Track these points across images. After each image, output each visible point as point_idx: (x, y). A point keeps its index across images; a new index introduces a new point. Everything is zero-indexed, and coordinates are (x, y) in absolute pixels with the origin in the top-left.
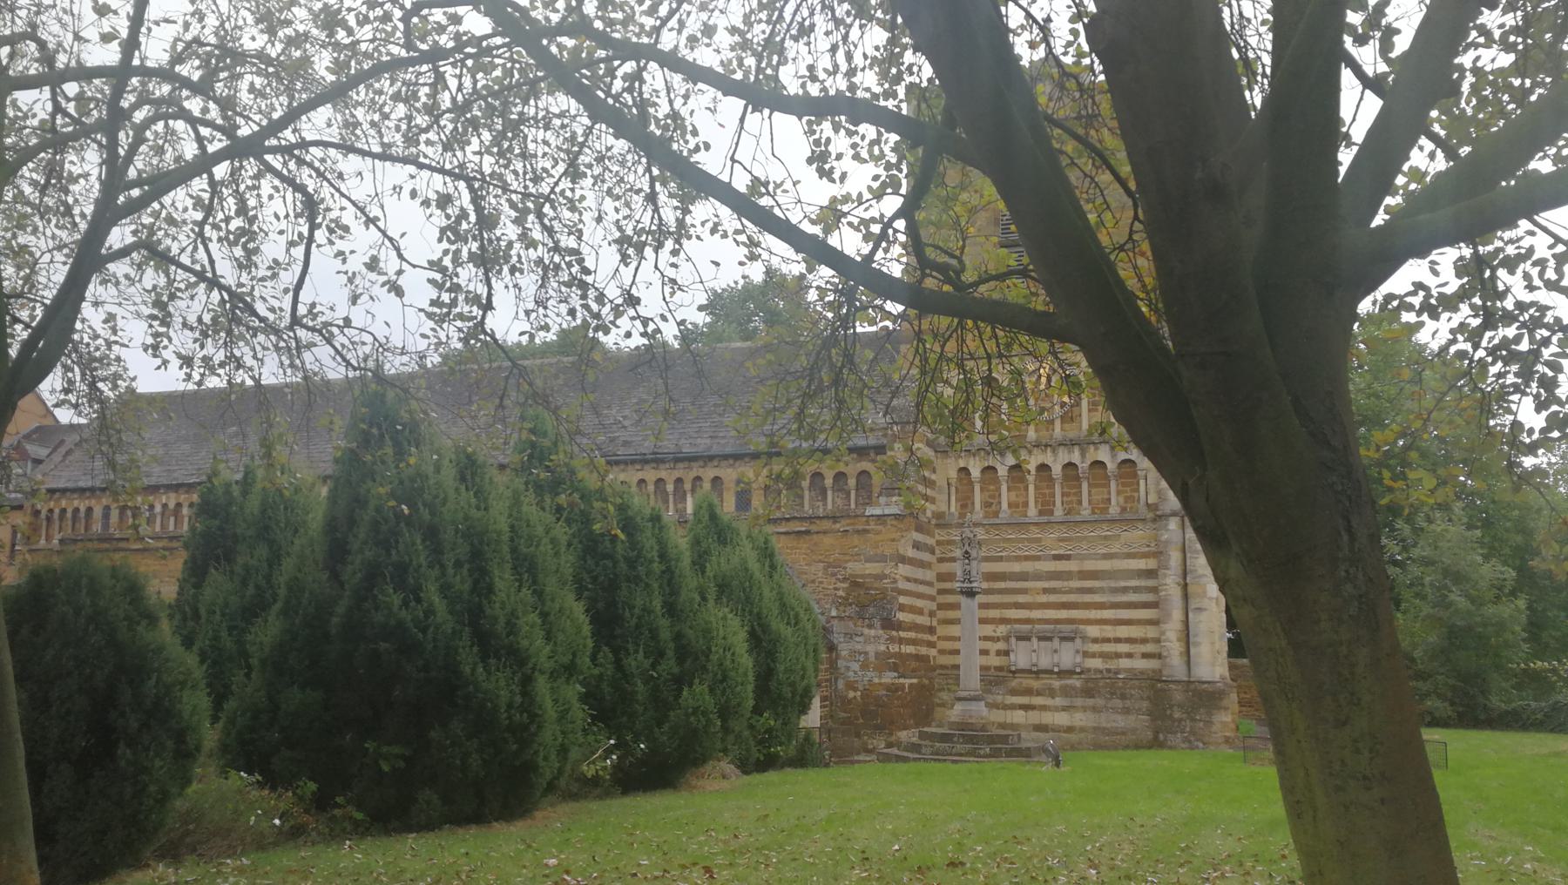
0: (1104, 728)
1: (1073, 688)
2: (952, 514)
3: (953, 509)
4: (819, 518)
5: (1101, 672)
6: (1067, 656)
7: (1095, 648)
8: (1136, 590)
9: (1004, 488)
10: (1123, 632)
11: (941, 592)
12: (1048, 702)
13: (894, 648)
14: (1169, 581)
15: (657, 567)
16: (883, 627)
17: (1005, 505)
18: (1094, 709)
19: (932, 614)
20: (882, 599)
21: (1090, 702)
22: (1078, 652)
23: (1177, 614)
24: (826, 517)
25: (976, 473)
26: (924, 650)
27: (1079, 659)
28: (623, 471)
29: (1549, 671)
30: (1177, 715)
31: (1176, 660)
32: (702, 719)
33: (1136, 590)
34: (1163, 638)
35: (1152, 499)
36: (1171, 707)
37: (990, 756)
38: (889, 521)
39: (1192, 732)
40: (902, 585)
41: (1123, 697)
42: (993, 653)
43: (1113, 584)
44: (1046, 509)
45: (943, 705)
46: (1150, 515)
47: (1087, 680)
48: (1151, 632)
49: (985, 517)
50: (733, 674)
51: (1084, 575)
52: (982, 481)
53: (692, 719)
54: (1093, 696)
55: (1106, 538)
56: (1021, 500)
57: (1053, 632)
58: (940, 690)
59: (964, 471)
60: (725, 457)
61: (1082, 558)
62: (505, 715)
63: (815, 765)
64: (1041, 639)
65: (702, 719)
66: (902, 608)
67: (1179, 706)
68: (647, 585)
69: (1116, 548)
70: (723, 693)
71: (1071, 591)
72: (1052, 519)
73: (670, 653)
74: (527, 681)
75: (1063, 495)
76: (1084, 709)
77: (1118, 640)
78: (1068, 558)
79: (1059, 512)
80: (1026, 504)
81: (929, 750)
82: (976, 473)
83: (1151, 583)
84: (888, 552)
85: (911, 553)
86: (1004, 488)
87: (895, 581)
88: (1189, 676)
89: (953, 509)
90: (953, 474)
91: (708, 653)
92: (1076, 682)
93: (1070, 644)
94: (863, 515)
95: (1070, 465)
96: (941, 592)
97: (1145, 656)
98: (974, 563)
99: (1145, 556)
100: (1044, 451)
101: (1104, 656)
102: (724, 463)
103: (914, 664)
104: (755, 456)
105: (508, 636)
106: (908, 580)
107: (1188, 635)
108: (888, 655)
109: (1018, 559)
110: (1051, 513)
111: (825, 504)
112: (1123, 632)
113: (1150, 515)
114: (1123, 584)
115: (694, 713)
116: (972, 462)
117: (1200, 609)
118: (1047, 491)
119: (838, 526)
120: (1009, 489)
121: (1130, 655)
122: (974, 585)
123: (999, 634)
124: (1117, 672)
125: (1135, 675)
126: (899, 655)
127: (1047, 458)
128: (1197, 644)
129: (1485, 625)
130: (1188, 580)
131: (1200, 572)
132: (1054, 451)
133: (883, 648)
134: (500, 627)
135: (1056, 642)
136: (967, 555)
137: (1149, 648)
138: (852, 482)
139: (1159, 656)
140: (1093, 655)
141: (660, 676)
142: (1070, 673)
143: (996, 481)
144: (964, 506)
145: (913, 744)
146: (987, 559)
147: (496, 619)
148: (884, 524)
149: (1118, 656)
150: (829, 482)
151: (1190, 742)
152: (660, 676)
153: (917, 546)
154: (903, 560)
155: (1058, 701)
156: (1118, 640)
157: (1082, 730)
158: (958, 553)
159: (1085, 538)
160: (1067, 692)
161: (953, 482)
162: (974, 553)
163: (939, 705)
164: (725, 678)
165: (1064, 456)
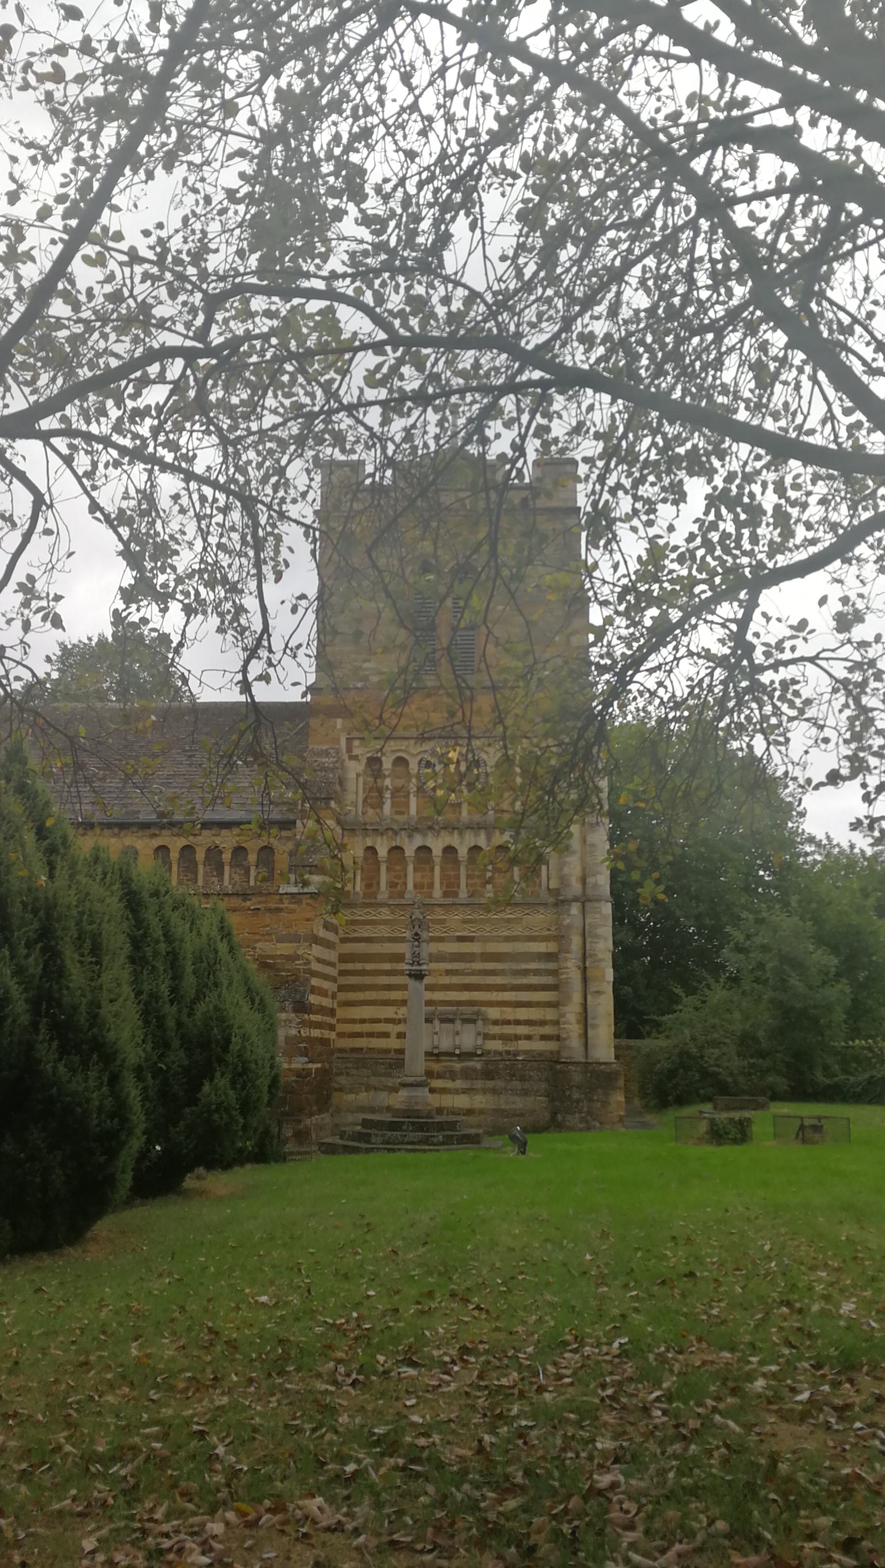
0: (503, 1110)
1: (474, 1070)
2: (356, 893)
3: (358, 889)
4: (227, 895)
5: (500, 1054)
6: (468, 1039)
7: (496, 1030)
8: (536, 972)
9: (410, 868)
10: (523, 1014)
11: (343, 973)
12: (450, 1084)
13: (305, 1032)
14: (569, 964)
15: (163, 947)
16: (295, 1011)
17: (410, 886)
18: (495, 1091)
19: (334, 996)
20: (294, 981)
21: (490, 1084)
22: (479, 1034)
23: (577, 997)
24: (236, 894)
25: (383, 852)
26: (327, 1034)
27: (480, 1041)
28: (115, 835)
29: (864, 1048)
30: (576, 1096)
31: (575, 1042)
32: (225, 1116)
33: (536, 972)
34: (562, 1020)
35: (553, 885)
36: (570, 1088)
37: (443, 1143)
38: (306, 900)
39: (590, 1113)
40: (316, 967)
41: (522, 1079)
42: (393, 1035)
43: (514, 966)
44: (450, 891)
45: (341, 1090)
46: (552, 900)
47: (487, 1063)
48: (550, 1014)
49: (390, 897)
50: (253, 1066)
51: (486, 957)
52: (389, 861)
53: (216, 1116)
54: (493, 1079)
55: (509, 921)
56: (426, 881)
57: (455, 1013)
58: (337, 1075)
59: (371, 850)
60: (109, 826)
61: (486, 940)
62: (96, 1122)
63: (241, 1159)
64: (442, 1021)
65: (225, 1116)
66: (314, 990)
67: (579, 1087)
68: (154, 967)
69: (517, 931)
70: (243, 1088)
71: (473, 973)
72: (457, 901)
73: (176, 1043)
74: (114, 1079)
75: (468, 877)
76: (484, 1091)
77: (518, 1022)
78: (471, 939)
79: (463, 894)
80: (431, 885)
81: (380, 1140)
82: (383, 852)
83: (551, 966)
84: (302, 932)
85: (322, 933)
86: (410, 868)
87: (308, 962)
88: (587, 1056)
89: (358, 889)
90: (360, 853)
91: (227, 1042)
92: (476, 1064)
93: (471, 1026)
94: (277, 893)
95: (476, 849)
96: (343, 973)
97: (544, 1038)
98: (424, 945)
99: (546, 939)
100: (451, 833)
101: (504, 1038)
102: (107, 832)
103: (319, 1048)
104: (145, 826)
105: (92, 1026)
106: (319, 960)
107: (586, 1018)
108: (299, 1039)
109: (508, 939)
110: (456, 895)
111: (221, 880)
112: (523, 1014)
113: (552, 900)
114: (524, 966)
115: (217, 1110)
116: (379, 839)
117: (598, 993)
118: (452, 873)
119: (248, 903)
120: (415, 870)
121: (528, 1038)
122: (424, 967)
123: (400, 1016)
124: (517, 1053)
125: (534, 1057)
126: (309, 1040)
127: (454, 840)
128: (595, 1026)
129: (815, 1007)
130: (588, 964)
131: (600, 956)
132: (461, 834)
133: (294, 1032)
134: (82, 1018)
135: (458, 1023)
136: (417, 937)
137: (548, 1030)
138: (252, 858)
139: (558, 1038)
140: (494, 1037)
141: (169, 1068)
142: (469, 1055)
143: (403, 861)
144: (368, 886)
145: (359, 1133)
146: (433, 939)
147: (75, 1008)
148: (299, 902)
149: (517, 1038)
150: (227, 856)
151: (587, 1122)
152: (169, 1068)
153: (327, 926)
154: (316, 940)
155: (459, 1084)
156: (518, 1022)
157: (482, 1112)
158: (408, 935)
159: (489, 920)
160: (467, 1074)
161: (360, 861)
162: (424, 935)
163: (336, 1090)
164: (245, 1070)
165: (470, 839)
